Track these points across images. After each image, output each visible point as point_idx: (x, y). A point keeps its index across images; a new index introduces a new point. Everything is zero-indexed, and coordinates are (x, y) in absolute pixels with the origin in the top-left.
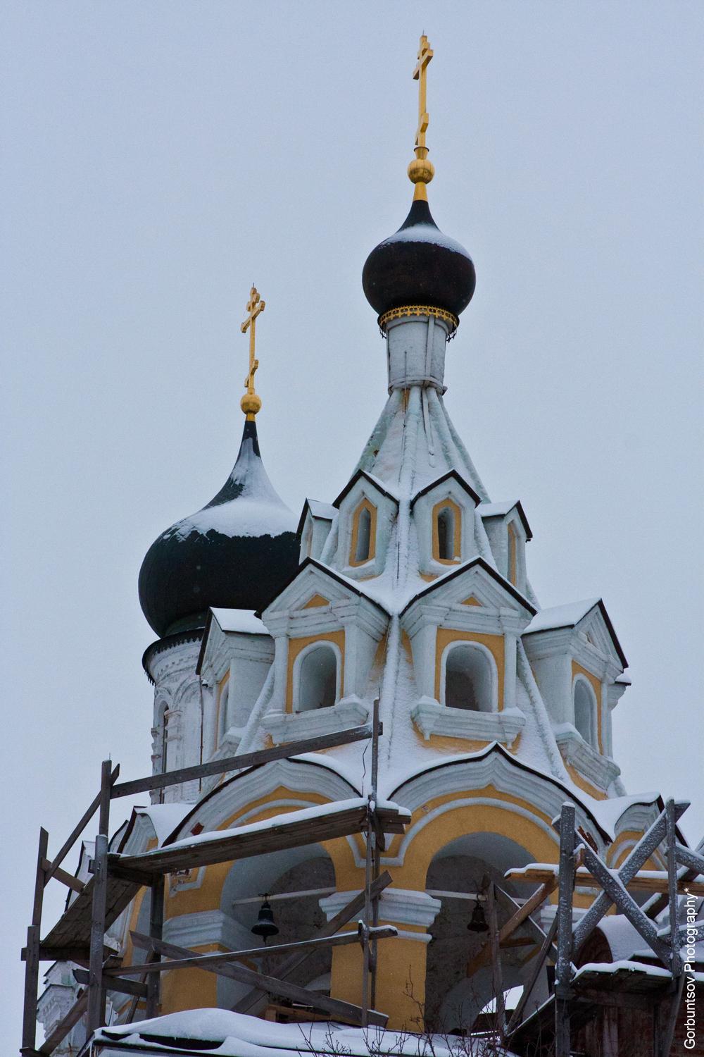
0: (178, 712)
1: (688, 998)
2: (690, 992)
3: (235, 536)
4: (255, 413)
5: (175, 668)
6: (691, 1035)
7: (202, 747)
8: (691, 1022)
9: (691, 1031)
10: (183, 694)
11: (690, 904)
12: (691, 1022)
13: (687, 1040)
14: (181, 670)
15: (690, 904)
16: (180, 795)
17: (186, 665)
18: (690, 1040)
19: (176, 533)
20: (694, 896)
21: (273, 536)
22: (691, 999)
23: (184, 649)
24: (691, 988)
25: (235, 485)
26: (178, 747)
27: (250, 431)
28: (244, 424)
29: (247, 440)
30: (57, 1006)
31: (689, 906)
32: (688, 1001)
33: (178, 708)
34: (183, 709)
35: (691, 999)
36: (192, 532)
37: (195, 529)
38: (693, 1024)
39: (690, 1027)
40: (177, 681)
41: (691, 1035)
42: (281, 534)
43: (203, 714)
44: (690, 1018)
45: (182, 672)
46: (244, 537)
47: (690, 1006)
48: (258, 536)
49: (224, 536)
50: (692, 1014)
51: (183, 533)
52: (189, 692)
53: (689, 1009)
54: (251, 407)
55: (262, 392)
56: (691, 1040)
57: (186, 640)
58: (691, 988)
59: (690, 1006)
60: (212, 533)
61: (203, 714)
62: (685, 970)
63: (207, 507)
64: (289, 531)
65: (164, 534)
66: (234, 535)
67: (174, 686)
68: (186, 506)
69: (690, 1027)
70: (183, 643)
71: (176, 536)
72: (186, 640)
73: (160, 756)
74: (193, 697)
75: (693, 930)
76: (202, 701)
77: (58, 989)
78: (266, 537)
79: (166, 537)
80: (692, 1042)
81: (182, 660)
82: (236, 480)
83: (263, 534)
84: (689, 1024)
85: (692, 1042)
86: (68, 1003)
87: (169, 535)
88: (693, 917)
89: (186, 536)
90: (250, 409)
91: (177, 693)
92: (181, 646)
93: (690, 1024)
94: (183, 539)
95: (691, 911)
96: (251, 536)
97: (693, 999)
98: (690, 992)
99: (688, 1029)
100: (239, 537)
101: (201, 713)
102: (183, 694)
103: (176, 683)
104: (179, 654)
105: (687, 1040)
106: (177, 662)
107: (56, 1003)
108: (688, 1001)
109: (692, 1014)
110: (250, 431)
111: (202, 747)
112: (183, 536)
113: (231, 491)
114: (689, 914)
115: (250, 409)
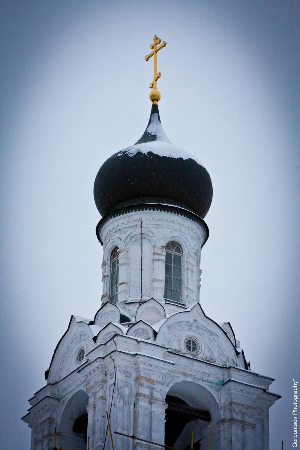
0: (128, 250)
1: (294, 426)
2: (295, 423)
3: (164, 157)
4: (158, 101)
5: (124, 226)
6: (295, 441)
7: (142, 270)
8: (295, 436)
9: (295, 440)
10: (130, 240)
11: (295, 386)
12: (295, 436)
13: (293, 444)
14: (128, 227)
15: (295, 386)
16: (128, 295)
17: (132, 225)
18: (295, 444)
19: (127, 153)
20: (297, 383)
21: (184, 159)
22: (295, 426)
23: (131, 215)
24: (295, 421)
25: (151, 135)
26: (127, 269)
27: (155, 109)
28: (151, 106)
29: (155, 114)
30: (48, 409)
31: (294, 386)
32: (294, 427)
33: (127, 248)
34: (129, 248)
35: (295, 426)
36: (138, 152)
37: (139, 151)
38: (296, 437)
39: (295, 438)
40: (125, 233)
41: (295, 441)
42: (188, 159)
43: (142, 252)
44: (295, 434)
45: (129, 228)
46: (169, 157)
47: (295, 429)
48: (177, 158)
49: (157, 156)
50: (296, 433)
51: (132, 153)
52: (133, 239)
53: (294, 430)
54: (156, 97)
55: (161, 88)
56: (296, 443)
57: (128, 212)
58: (295, 421)
59: (295, 429)
60: (150, 153)
61: (142, 252)
62: (293, 414)
63: (136, 144)
64: (192, 158)
65: (119, 153)
66: (163, 156)
67: (124, 236)
68: (127, 141)
69: (295, 438)
70: (132, 211)
71: (127, 154)
72: (134, 210)
73: (108, 276)
74: (135, 242)
75: (296, 397)
76: (141, 245)
77: (51, 399)
78: (181, 159)
79: (119, 155)
80: (296, 444)
81: (129, 222)
82: (151, 133)
83: (179, 157)
84: (294, 437)
85: (296, 444)
86: (55, 408)
87: (122, 154)
88: (296, 391)
89: (134, 154)
90: (155, 98)
91: (126, 240)
92: (131, 213)
93: (295, 436)
94: (132, 155)
95: (295, 389)
96: (173, 157)
97: (296, 426)
98: (295, 423)
99: (294, 439)
100: (166, 157)
101: (141, 251)
102: (130, 240)
103: (124, 235)
104: (127, 218)
105: (293, 444)
106: (126, 223)
107: (47, 408)
108: (294, 427)
109: (296, 433)
110: (155, 109)
111: (142, 270)
112: (132, 154)
113: (148, 137)
114: (294, 390)
115: (155, 98)
